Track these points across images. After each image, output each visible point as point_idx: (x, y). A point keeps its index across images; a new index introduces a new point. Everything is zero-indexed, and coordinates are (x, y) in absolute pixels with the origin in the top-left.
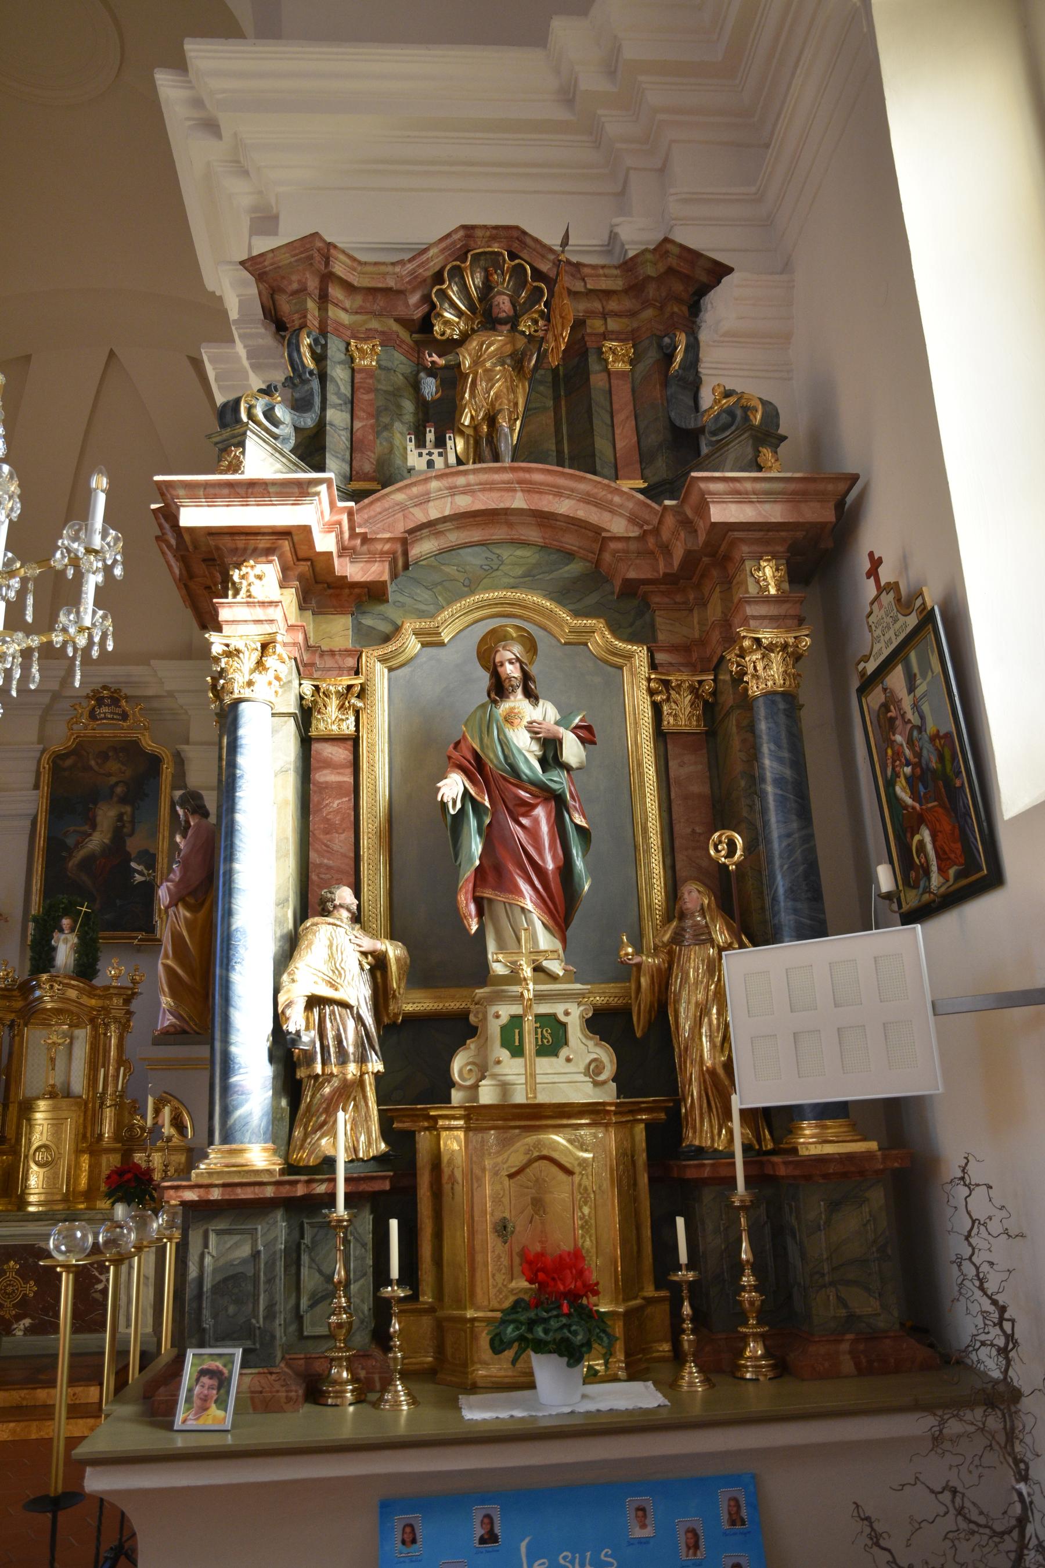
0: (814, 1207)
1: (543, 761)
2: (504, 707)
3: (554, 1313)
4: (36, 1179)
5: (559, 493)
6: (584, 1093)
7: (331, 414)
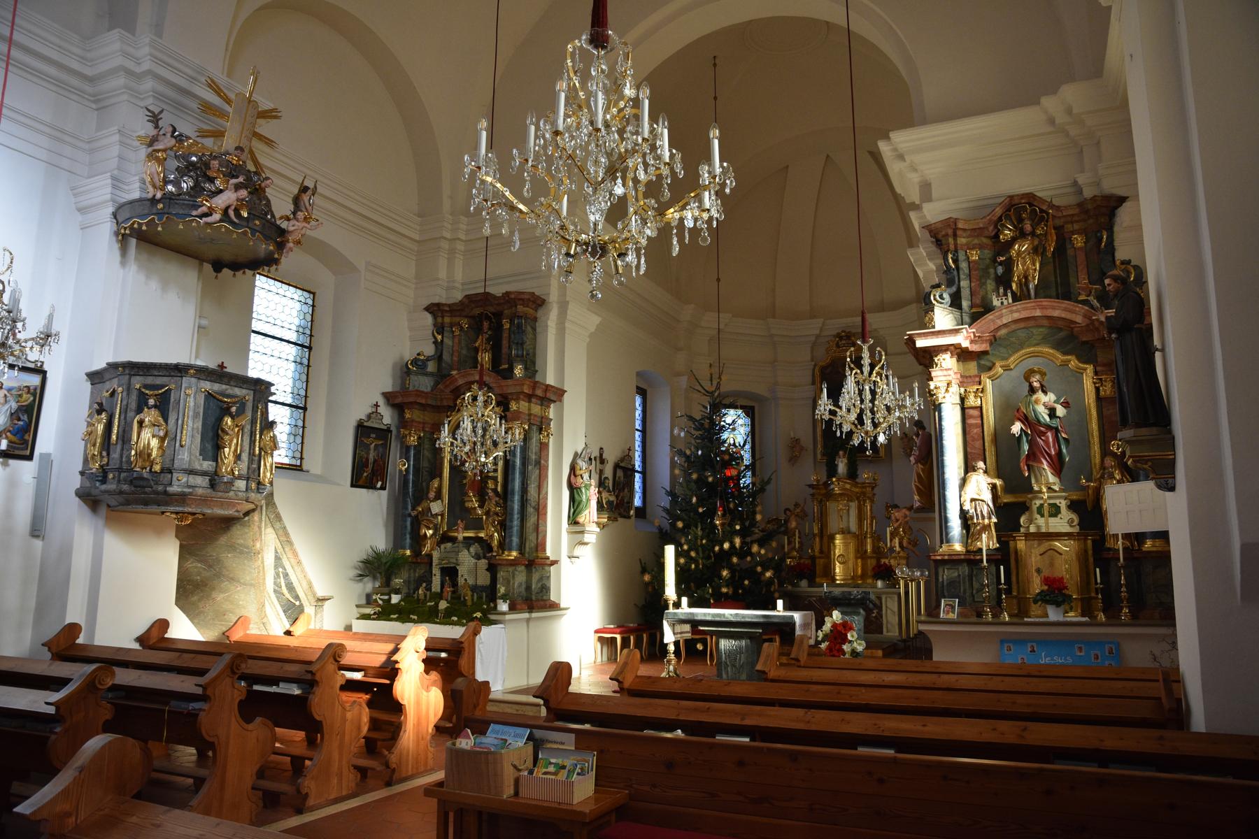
2: (1035, 397)
3: (1055, 593)
4: (838, 569)
5: (1054, 308)
6: (1066, 529)
7: (962, 283)
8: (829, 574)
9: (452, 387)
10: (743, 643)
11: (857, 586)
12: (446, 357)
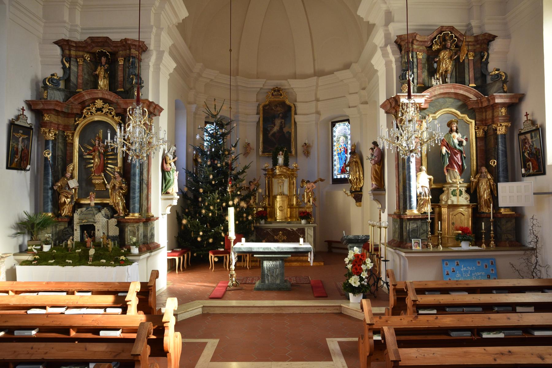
0: (503, 222)
1: (459, 145)
5: (460, 89)
8: (273, 214)
9: (80, 101)
10: (278, 263)
11: (289, 223)
12: (73, 79)
